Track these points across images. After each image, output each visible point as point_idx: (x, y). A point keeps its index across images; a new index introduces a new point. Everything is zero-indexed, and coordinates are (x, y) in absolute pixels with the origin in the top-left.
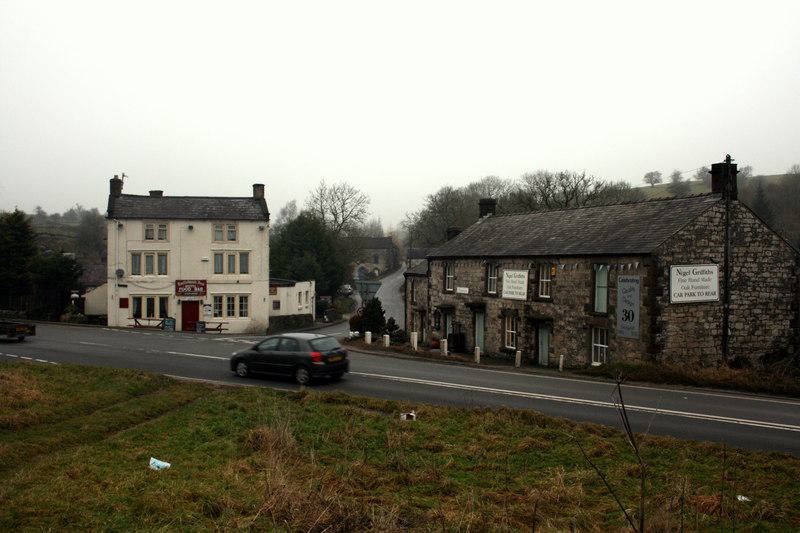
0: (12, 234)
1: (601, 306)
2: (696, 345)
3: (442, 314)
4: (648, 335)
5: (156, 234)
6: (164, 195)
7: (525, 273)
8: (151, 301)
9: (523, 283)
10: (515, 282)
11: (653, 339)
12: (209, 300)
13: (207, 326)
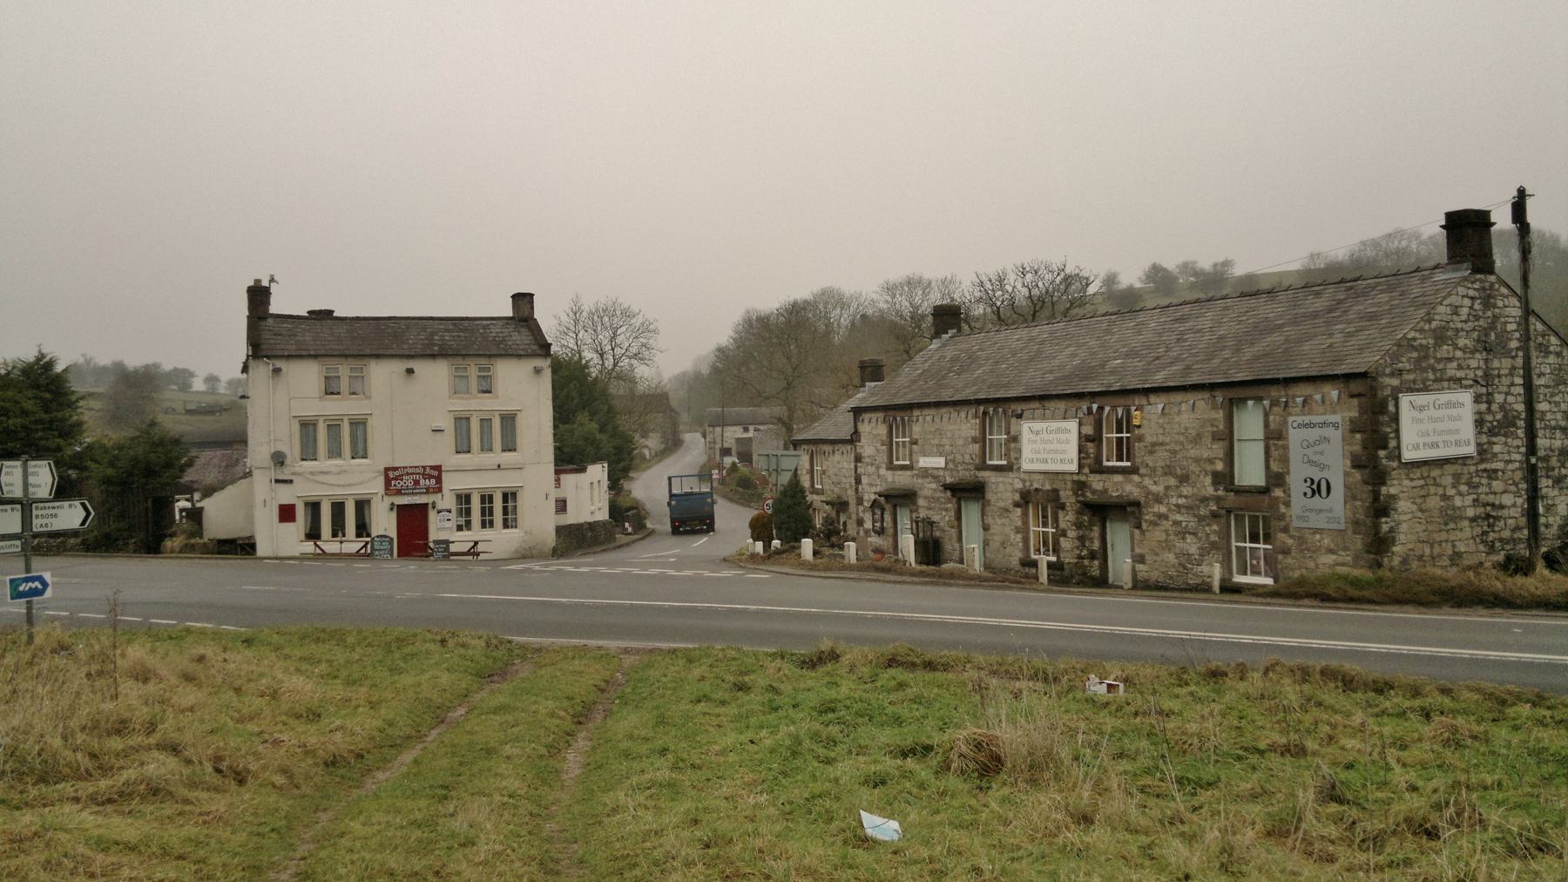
0: (35, 398)
1: (1250, 471)
2: (1444, 536)
3: (888, 507)
4: (1368, 521)
5: (344, 386)
6: (335, 315)
7: (1073, 425)
8: (338, 509)
9: (1068, 442)
10: (1436, 420)
11: (1376, 527)
12: (447, 501)
13: (453, 548)
